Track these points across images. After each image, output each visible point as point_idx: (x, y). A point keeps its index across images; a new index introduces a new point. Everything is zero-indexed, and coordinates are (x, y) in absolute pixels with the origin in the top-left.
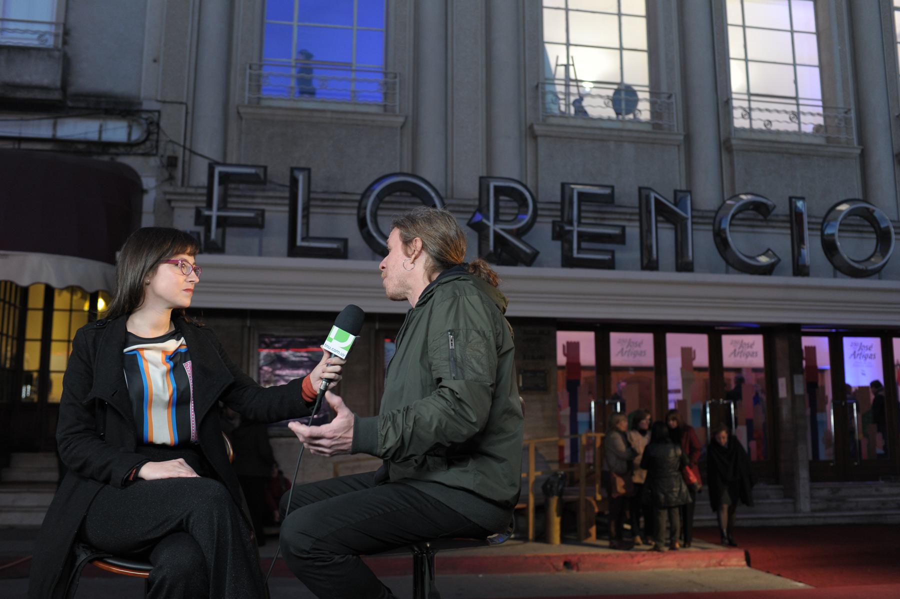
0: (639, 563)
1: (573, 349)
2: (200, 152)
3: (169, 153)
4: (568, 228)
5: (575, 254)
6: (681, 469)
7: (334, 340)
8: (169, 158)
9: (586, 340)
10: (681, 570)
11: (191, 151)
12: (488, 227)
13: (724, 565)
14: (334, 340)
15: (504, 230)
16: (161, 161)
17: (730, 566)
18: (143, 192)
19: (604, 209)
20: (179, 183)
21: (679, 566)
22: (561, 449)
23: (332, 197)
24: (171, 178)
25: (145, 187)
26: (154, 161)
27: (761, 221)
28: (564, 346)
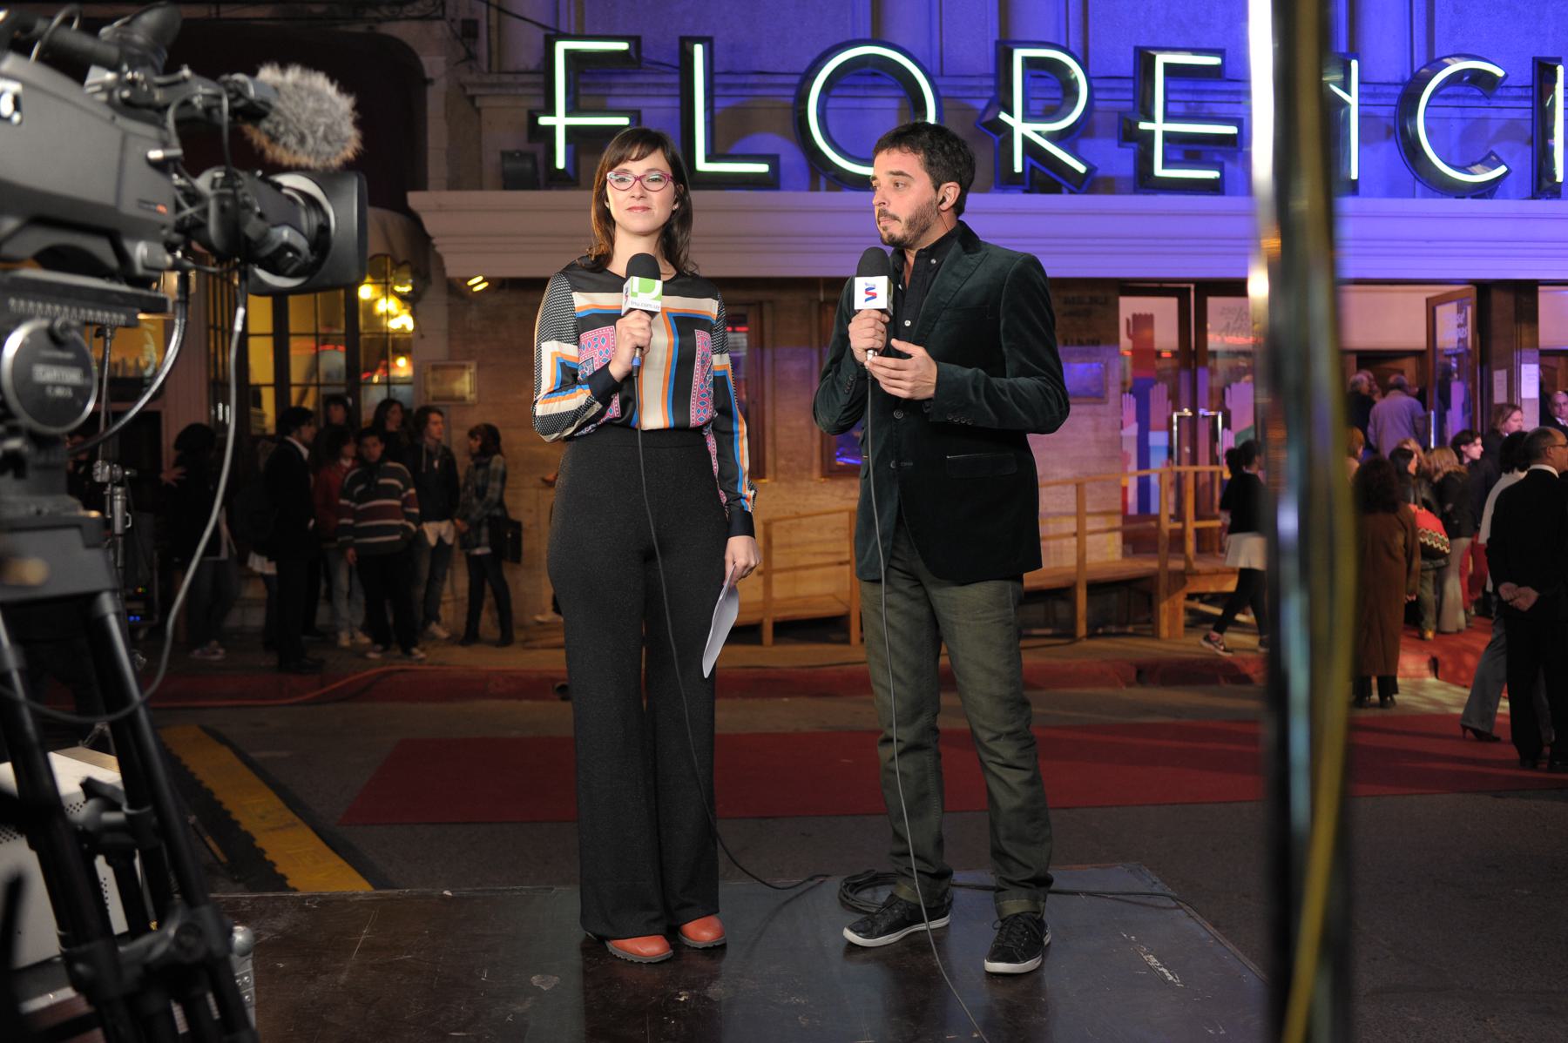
1: (1143, 322)
2: (516, 11)
3: (464, 14)
4: (1143, 126)
5: (1159, 171)
7: (639, 294)
8: (465, 22)
9: (1164, 311)
11: (500, 9)
12: (1009, 130)
14: (639, 294)
15: (1038, 133)
16: (452, 30)
18: (427, 82)
20: (485, 67)
22: (1125, 490)
23: (742, 80)
24: (471, 57)
25: (428, 75)
26: (439, 29)
27: (1478, 98)
28: (1128, 321)
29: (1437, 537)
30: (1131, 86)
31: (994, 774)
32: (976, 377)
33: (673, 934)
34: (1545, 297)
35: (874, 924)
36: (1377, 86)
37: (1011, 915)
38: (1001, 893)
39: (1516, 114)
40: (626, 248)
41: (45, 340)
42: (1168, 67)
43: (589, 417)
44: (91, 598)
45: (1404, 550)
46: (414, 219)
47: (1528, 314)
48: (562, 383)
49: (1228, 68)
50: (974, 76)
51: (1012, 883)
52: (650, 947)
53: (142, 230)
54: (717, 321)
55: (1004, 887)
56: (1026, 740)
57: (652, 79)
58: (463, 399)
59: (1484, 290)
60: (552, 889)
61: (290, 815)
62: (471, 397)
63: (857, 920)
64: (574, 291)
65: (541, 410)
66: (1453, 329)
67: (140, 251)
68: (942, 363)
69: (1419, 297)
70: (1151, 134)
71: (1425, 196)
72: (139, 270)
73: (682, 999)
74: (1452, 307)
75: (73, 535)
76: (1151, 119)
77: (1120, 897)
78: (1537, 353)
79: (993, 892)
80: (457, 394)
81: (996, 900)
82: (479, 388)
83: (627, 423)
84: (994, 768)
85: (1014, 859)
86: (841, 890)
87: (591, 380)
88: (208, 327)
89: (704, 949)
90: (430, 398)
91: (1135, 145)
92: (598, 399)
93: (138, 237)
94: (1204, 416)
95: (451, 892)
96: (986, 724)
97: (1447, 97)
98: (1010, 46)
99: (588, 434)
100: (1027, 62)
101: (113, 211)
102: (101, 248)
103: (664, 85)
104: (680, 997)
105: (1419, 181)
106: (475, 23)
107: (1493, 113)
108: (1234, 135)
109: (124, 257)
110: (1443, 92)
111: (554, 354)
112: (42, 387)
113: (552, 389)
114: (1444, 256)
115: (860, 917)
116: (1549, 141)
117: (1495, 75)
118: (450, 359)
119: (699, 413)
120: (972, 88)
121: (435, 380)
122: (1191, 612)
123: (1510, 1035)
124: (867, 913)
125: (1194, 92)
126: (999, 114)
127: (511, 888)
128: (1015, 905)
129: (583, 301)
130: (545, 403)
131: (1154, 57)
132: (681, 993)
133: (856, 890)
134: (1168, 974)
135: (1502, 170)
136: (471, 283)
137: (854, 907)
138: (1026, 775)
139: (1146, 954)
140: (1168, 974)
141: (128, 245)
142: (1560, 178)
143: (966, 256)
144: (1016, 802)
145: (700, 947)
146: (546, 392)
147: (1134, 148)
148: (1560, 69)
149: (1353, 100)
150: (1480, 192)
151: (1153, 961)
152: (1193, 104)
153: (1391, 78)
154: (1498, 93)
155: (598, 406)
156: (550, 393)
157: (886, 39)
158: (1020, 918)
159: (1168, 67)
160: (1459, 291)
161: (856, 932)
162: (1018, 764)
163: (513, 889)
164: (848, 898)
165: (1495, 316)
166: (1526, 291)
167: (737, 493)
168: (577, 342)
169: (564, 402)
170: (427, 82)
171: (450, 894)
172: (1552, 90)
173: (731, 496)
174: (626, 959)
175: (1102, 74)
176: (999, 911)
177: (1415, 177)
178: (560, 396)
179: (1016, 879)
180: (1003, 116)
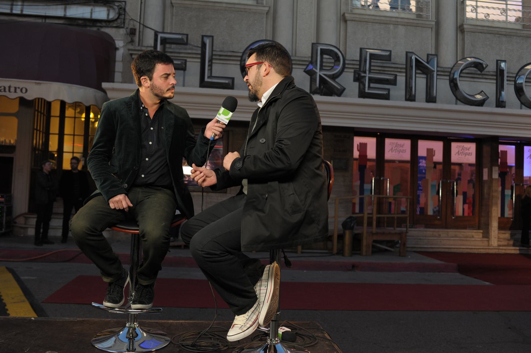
1: (363, 147)
9: (371, 143)
11: (143, 25)
15: (324, 75)
16: (126, 31)
18: (117, 49)
22: (354, 204)
24: (132, 41)
25: (117, 46)
26: (122, 31)
28: (358, 145)
45: (273, 103)
46: (104, 91)
61: (24, 298)
88: (34, 129)
106: (135, 30)
122: (373, 246)
170: (117, 49)
175: (350, 59)
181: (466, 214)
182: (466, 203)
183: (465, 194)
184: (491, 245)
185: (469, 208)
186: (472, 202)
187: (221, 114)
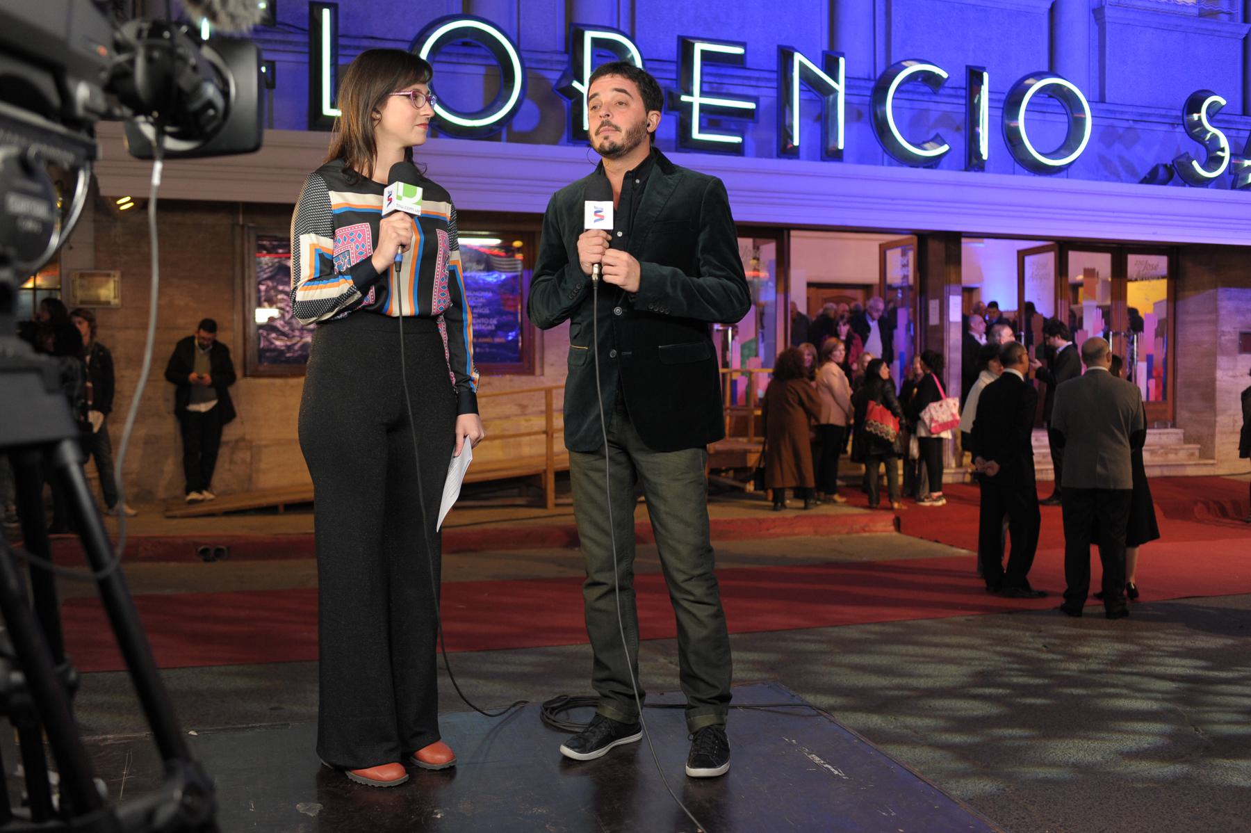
0: (768, 530)
4: (684, 98)
5: (696, 135)
6: (55, 259)
10: (818, 537)
13: (868, 531)
17: (876, 531)
19: (723, 71)
21: (816, 532)
29: (877, 426)
30: (675, 68)
31: (689, 612)
32: (675, 275)
33: (407, 759)
34: (967, 246)
35: (586, 740)
36: (851, 80)
37: (703, 728)
38: (692, 710)
39: (948, 108)
40: (388, 155)
41: (15, 168)
42: (704, 53)
43: (347, 305)
44: (50, 448)
47: (954, 259)
48: (320, 273)
49: (749, 59)
50: (546, 52)
51: (701, 701)
52: (390, 773)
53: (86, 70)
54: (451, 222)
55: (694, 704)
56: (711, 579)
57: (278, 37)
58: (108, 303)
59: (923, 238)
60: (288, 724)
62: (115, 302)
63: (569, 739)
64: (330, 190)
65: (301, 296)
66: (900, 269)
67: (82, 92)
68: (645, 263)
69: (873, 242)
70: (690, 105)
71: (890, 164)
72: (80, 111)
73: (439, 816)
74: (898, 251)
75: (32, 380)
76: (690, 93)
77: (771, 708)
78: (960, 289)
79: (684, 710)
80: (103, 299)
81: (687, 716)
82: (122, 293)
83: (379, 311)
84: (686, 604)
85: (703, 680)
86: (543, 714)
87: (353, 271)
89: (441, 770)
90: (78, 301)
91: (676, 113)
92: (359, 289)
93: (81, 77)
94: (718, 330)
95: (196, 732)
96: (682, 567)
97: (908, 92)
98: (582, 28)
99: (343, 318)
100: (595, 41)
101: (62, 44)
102: (44, 82)
103: (290, 43)
104: (437, 814)
105: (887, 154)
107: (932, 106)
108: (753, 110)
109: (66, 97)
110: (903, 88)
111: (312, 245)
112: (15, 218)
113: (312, 277)
114: (889, 210)
115: (571, 736)
116: (977, 129)
117: (941, 76)
118: (96, 269)
119: (439, 301)
120: (545, 61)
121: (82, 286)
123: (1025, 800)
124: (576, 732)
125: (716, 75)
126: (572, 82)
127: (250, 725)
128: (704, 720)
129: (340, 199)
130: (306, 290)
131: (693, 44)
132: (435, 811)
133: (554, 713)
134: (833, 770)
135: (945, 148)
136: (119, 202)
137: (559, 728)
138: (712, 610)
139: (810, 754)
140: (833, 770)
141: (70, 83)
142: (985, 157)
143: (665, 176)
144: (704, 633)
145: (438, 769)
146: (306, 279)
147: (676, 116)
148: (986, 76)
149: (840, 87)
150: (929, 164)
151: (817, 759)
152: (715, 85)
153: (861, 75)
154: (941, 92)
155: (358, 295)
156: (309, 281)
157: (479, 15)
158: (709, 730)
159: (704, 53)
160: (906, 239)
161: (573, 748)
162: (706, 600)
163: (253, 727)
164: (549, 718)
165: (931, 258)
166: (953, 240)
167: (467, 376)
168: (333, 235)
169: (325, 291)
171: (195, 734)
172: (979, 91)
173: (461, 377)
174: (367, 785)
176: (690, 727)
177: (884, 150)
178: (322, 284)
179: (704, 697)
180: (576, 84)
181: (1152, 398)
182: (1152, 377)
183: (1149, 359)
184: (948, 464)
185: (1157, 386)
186: (1162, 375)
187: (401, 197)
